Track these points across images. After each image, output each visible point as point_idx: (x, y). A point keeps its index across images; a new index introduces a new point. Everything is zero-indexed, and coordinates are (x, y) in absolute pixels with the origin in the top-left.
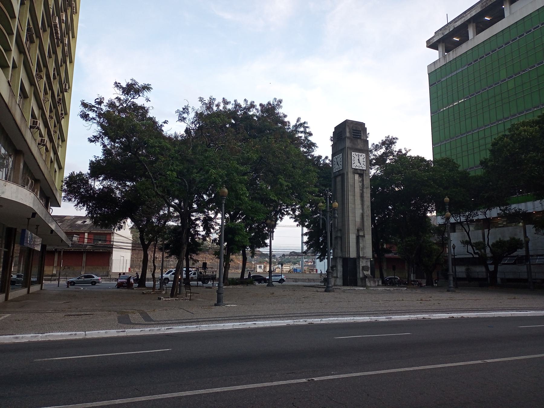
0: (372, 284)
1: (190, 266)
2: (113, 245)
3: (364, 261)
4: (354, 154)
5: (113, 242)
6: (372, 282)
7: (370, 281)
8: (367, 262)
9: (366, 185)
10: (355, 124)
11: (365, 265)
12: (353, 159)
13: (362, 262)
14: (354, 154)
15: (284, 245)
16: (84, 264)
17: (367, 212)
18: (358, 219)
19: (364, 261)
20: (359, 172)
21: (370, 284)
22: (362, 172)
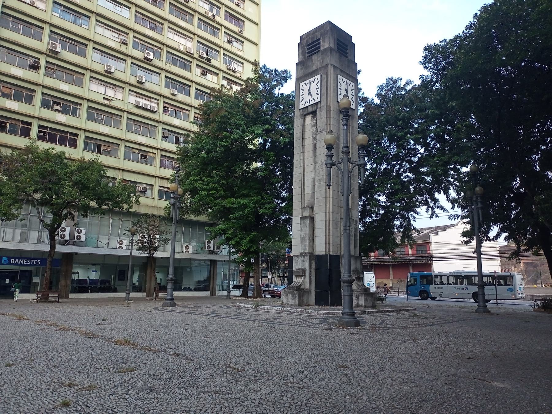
0: (290, 301)
1: (129, 254)
2: (432, 256)
3: (299, 260)
4: (340, 79)
5: (432, 250)
6: (290, 296)
7: (287, 295)
8: (303, 261)
9: (320, 127)
10: (313, 34)
11: (301, 267)
12: (339, 87)
13: (297, 262)
14: (340, 79)
15: (352, 242)
16: (391, 277)
17: (321, 173)
18: (308, 190)
19: (299, 260)
20: (310, 110)
21: (287, 299)
22: (315, 108)
